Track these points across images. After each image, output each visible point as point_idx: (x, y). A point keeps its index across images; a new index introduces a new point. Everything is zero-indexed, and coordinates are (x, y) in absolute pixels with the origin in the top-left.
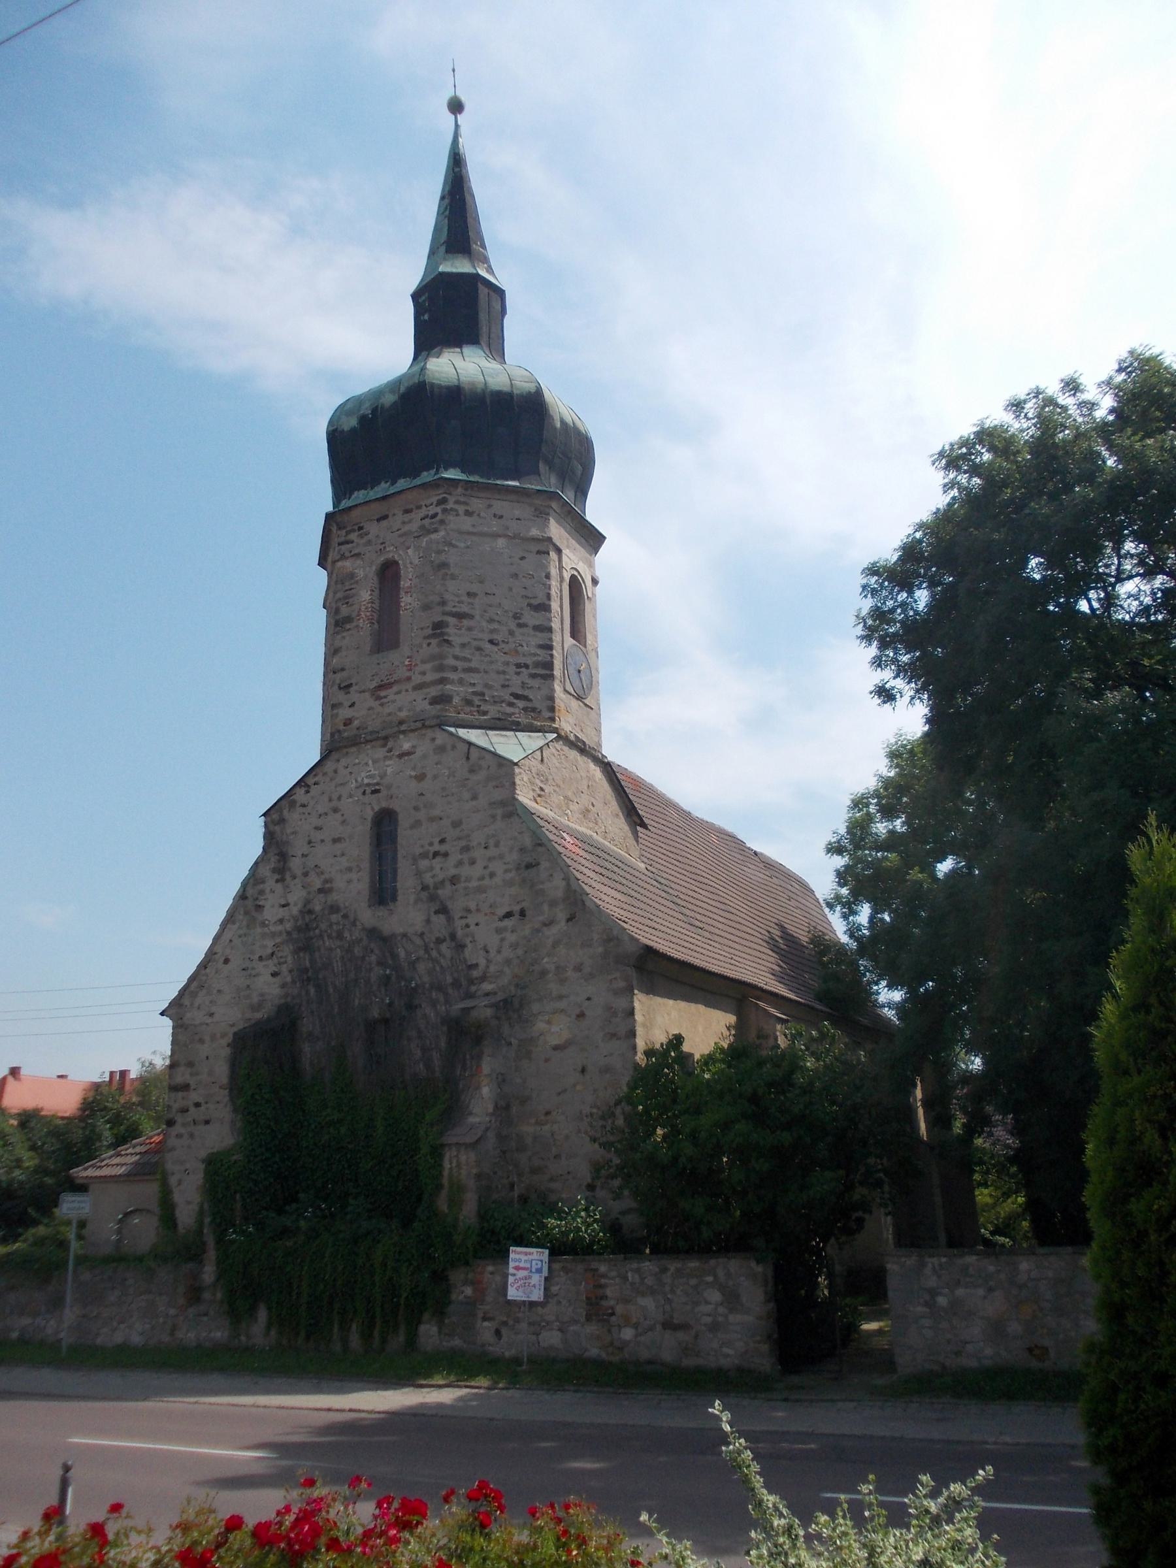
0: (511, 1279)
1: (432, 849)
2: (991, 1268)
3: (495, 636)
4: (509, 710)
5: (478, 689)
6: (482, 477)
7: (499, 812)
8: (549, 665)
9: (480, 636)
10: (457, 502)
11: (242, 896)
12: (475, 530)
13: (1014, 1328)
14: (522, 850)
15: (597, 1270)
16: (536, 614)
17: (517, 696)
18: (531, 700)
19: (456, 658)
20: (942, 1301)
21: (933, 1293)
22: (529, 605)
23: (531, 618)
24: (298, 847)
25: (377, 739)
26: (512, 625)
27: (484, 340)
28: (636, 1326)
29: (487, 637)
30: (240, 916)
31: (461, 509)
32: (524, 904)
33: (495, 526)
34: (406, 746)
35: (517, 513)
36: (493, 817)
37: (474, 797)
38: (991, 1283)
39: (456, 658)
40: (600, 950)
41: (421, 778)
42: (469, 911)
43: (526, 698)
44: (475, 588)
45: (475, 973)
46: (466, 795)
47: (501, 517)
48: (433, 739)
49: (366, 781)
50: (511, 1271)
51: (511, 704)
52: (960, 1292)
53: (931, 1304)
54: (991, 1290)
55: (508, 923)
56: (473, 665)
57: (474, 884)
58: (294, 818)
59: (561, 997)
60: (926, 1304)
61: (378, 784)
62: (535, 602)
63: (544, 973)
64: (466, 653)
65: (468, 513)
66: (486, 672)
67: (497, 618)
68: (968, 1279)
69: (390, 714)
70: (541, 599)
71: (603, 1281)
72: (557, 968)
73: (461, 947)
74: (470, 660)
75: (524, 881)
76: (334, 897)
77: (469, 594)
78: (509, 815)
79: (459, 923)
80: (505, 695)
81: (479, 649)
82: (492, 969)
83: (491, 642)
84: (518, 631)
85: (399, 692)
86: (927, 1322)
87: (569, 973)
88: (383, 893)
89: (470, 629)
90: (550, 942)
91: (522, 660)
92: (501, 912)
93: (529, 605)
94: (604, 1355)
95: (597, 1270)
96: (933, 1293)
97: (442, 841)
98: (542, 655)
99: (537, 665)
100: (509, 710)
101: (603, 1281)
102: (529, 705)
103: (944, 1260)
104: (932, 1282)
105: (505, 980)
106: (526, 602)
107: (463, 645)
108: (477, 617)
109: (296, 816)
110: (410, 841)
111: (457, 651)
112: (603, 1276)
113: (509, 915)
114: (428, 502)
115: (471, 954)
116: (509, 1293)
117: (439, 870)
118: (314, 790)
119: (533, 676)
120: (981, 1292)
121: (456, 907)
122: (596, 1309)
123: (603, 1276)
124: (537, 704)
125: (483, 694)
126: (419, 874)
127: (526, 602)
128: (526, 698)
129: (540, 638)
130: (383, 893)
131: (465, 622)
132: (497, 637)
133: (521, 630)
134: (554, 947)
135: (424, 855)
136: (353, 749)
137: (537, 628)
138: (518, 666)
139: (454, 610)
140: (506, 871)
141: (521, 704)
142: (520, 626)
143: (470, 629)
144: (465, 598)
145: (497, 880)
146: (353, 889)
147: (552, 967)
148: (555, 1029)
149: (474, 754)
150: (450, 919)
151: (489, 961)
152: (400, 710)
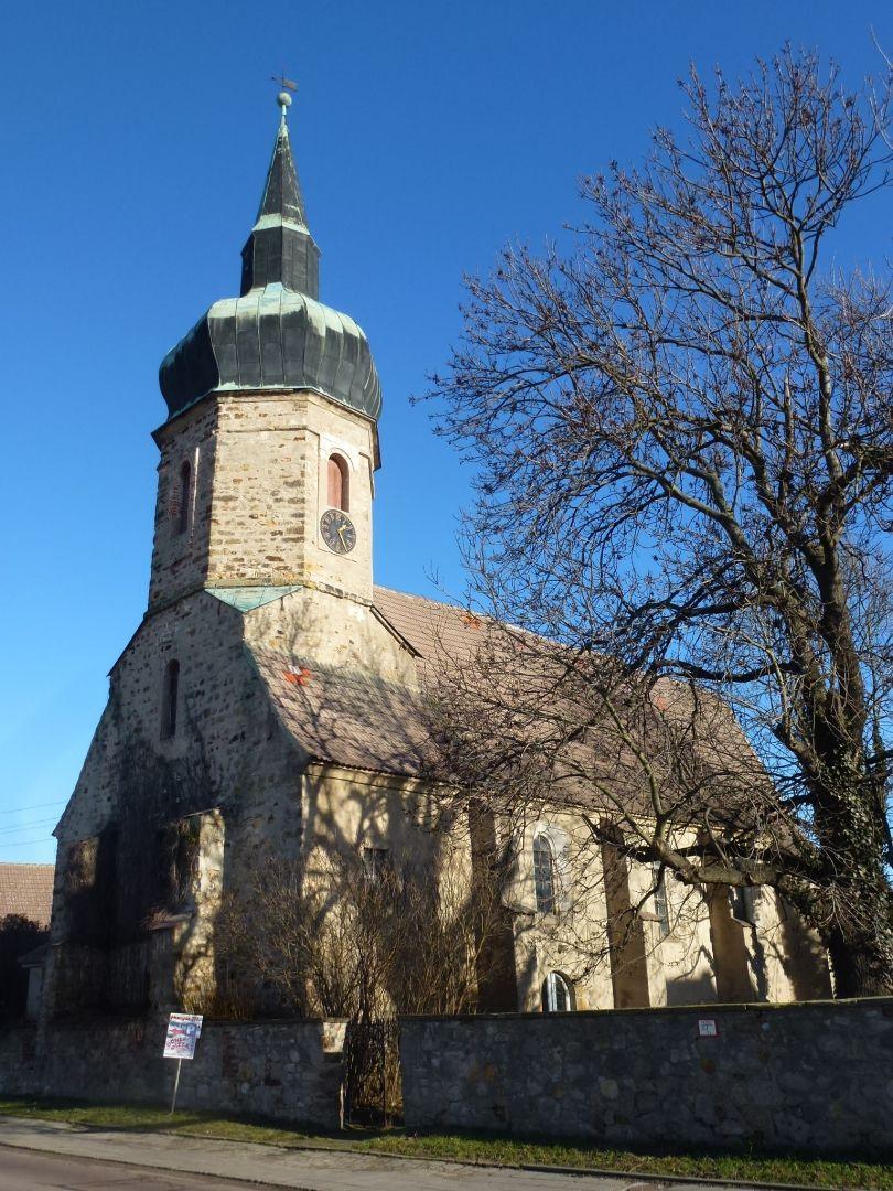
0: (168, 1039)
1: (196, 689)
2: (468, 1032)
3: (255, 511)
4: (264, 570)
5: (239, 556)
6: (252, 385)
7: (234, 654)
8: (300, 530)
9: (243, 512)
10: (230, 409)
11: (96, 739)
12: (242, 429)
13: (482, 1088)
14: (246, 684)
15: (229, 1033)
16: (290, 490)
17: (272, 559)
18: (283, 560)
19: (221, 533)
20: (435, 1062)
21: (429, 1054)
22: (286, 483)
23: (287, 493)
24: (126, 697)
25: (171, 606)
26: (270, 501)
27: (286, 277)
28: (249, 1081)
29: (248, 512)
30: (94, 755)
31: (232, 414)
32: (244, 729)
33: (261, 423)
34: (186, 608)
35: (279, 411)
36: (231, 659)
37: (221, 645)
38: (469, 1046)
39: (221, 533)
40: (285, 762)
41: (192, 633)
42: (213, 737)
43: (280, 559)
44: (241, 475)
45: (215, 788)
46: (217, 644)
47: (265, 415)
48: (201, 601)
49: (164, 640)
50: (169, 1033)
51: (266, 566)
52: (447, 1054)
53: (428, 1064)
54: (467, 1053)
55: (235, 744)
56: (234, 537)
57: (217, 715)
58: (124, 673)
59: (260, 804)
60: (424, 1066)
61: (170, 641)
62: (290, 480)
63: (252, 784)
64: (230, 528)
65: (237, 416)
66: (246, 541)
67: (257, 497)
68: (453, 1043)
69: (180, 584)
70: (296, 476)
71: (233, 1042)
72: (260, 779)
73: (207, 767)
74: (233, 534)
75: (245, 709)
76: (143, 734)
77: (235, 481)
78: (240, 656)
79: (208, 748)
80: (261, 558)
81: (241, 524)
82: (224, 784)
83: (252, 517)
84: (275, 506)
85: (185, 567)
86: (424, 1081)
87: (267, 784)
88: (169, 730)
89: (234, 509)
90: (256, 758)
91: (277, 529)
92: (231, 737)
93: (286, 483)
94: (231, 1106)
95: (229, 1033)
96: (429, 1054)
97: (202, 682)
98: (296, 522)
99: (289, 531)
100: (264, 570)
101: (233, 1042)
102: (281, 564)
103: (437, 1024)
104: (429, 1045)
105: (229, 793)
106: (283, 480)
107: (228, 523)
108: (241, 498)
109: (127, 672)
110: (184, 680)
111: (222, 528)
112: (233, 1038)
113: (235, 738)
114: (209, 412)
115: (215, 775)
116: (166, 1051)
117: (201, 704)
118: (137, 650)
119: (286, 540)
120: (461, 1054)
121: (206, 734)
122: (229, 1066)
123: (233, 1038)
124: (288, 563)
125: (242, 560)
126: (188, 710)
127: (283, 480)
128: (280, 559)
129: (294, 508)
130: (169, 730)
131: (231, 504)
132: (257, 512)
133: (278, 504)
134: (259, 762)
135: (191, 696)
136: (158, 616)
137: (292, 501)
138: (274, 534)
139: (222, 495)
140: (236, 702)
141: (275, 564)
142: (277, 500)
143: (234, 509)
144: (231, 485)
145: (230, 709)
146: (153, 727)
147: (256, 779)
148: (257, 831)
149: (223, 609)
150: (202, 746)
151: (222, 777)
152: (185, 580)
